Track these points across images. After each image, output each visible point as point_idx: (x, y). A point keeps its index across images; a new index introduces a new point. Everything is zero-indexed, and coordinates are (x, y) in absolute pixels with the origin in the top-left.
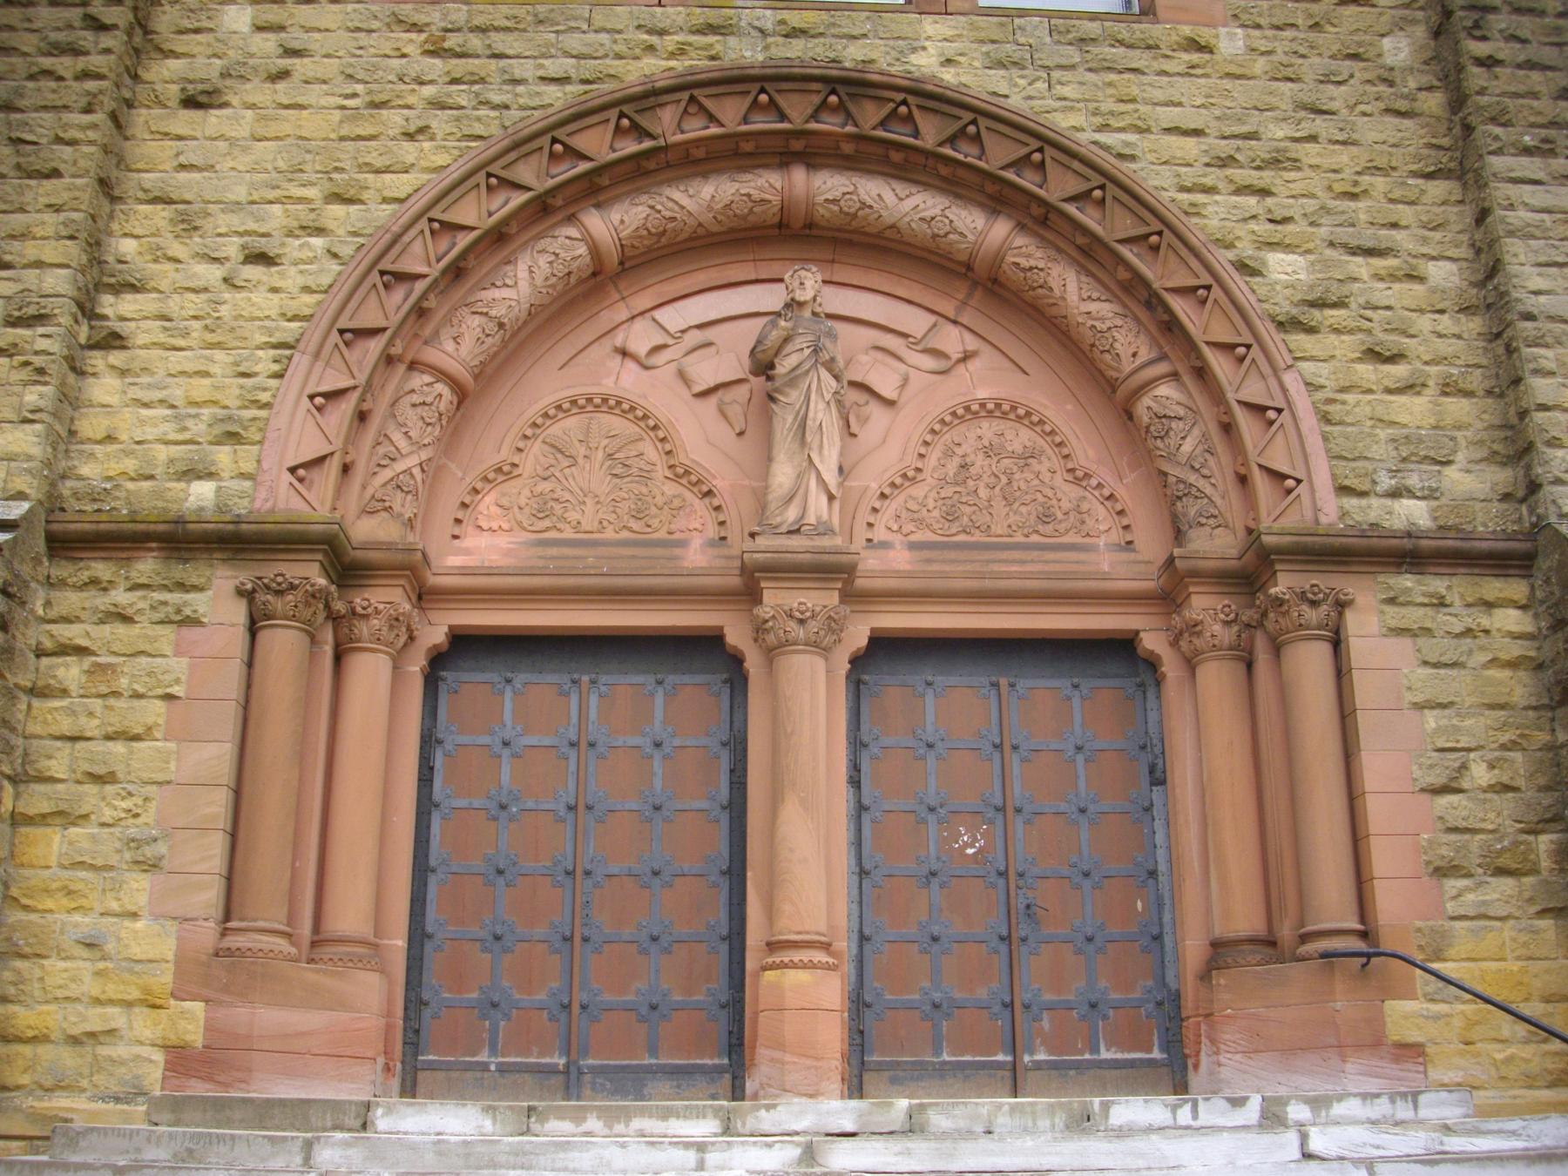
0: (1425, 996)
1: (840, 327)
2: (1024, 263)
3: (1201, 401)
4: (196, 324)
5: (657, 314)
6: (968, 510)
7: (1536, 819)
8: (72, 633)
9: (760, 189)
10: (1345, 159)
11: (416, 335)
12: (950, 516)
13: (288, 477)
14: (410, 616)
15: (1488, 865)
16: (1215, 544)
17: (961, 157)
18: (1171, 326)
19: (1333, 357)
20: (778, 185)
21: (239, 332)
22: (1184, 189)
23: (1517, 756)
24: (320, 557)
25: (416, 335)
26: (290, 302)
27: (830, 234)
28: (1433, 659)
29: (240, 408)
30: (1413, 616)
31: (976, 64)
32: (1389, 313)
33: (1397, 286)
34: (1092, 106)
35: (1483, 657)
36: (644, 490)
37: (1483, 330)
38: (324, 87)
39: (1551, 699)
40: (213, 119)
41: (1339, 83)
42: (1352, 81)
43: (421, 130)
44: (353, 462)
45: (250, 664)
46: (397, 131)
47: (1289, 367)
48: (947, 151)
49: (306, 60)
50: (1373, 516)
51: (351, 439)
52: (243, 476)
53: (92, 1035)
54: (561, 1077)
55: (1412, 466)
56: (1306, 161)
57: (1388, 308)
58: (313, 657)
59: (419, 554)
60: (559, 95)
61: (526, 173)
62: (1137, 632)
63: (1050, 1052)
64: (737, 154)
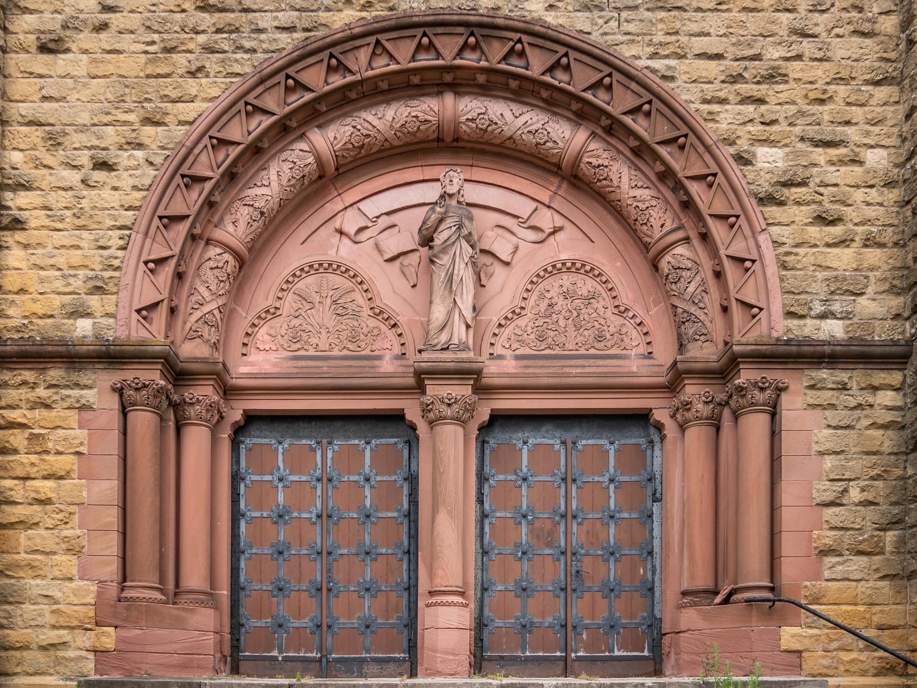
0: (805, 624)
1: (475, 212)
2: (595, 162)
4: (68, 213)
5: (361, 205)
6: (552, 334)
7: (886, 522)
8: (14, 415)
9: (424, 112)
10: (820, 72)
11: (209, 221)
12: (541, 338)
13: (135, 316)
14: (218, 404)
15: (853, 549)
16: (705, 353)
17: (556, 83)
18: (688, 205)
19: (793, 222)
20: (436, 109)
21: (96, 219)
22: (705, 101)
23: (880, 484)
24: (160, 367)
25: (209, 221)
26: (126, 197)
27: (470, 145)
28: (834, 424)
29: (102, 270)
30: (825, 396)
31: (570, 8)
32: (835, 189)
33: (843, 169)
34: (647, 38)
35: (866, 422)
36: (356, 324)
37: (899, 199)
38: (132, 36)
39: (907, 448)
40: (61, 62)
41: (823, 11)
42: (832, 10)
43: (200, 69)
44: (176, 306)
45: (125, 433)
46: (184, 70)
47: (763, 230)
48: (547, 78)
49: (118, 15)
50: (807, 331)
51: (174, 291)
52: (108, 315)
53: (53, 645)
54: (318, 664)
55: (837, 297)
56: (792, 75)
57: (836, 185)
58: (162, 429)
59: (221, 365)
60: (289, 41)
61: (270, 101)
62: (651, 410)
63: (586, 651)
64: (409, 86)
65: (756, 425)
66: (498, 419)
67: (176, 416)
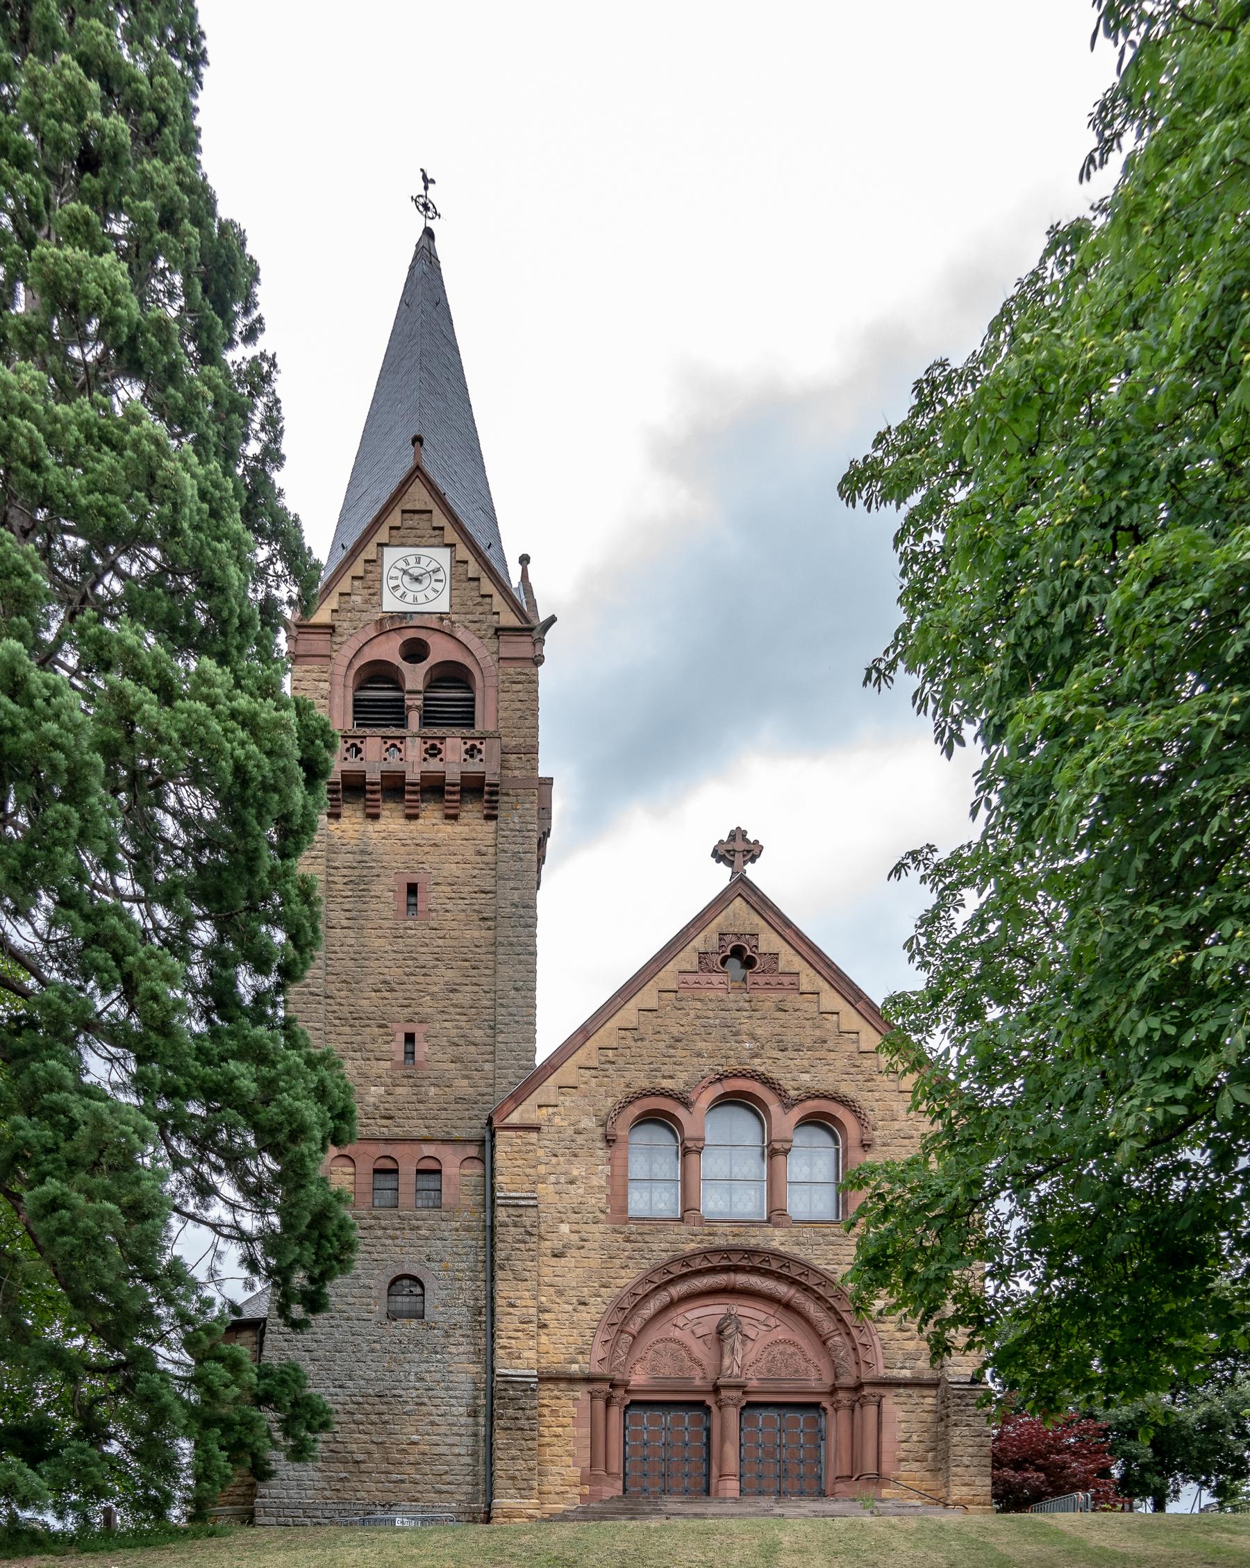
3: (847, 1341)
8: (545, 1402)
12: (769, 1371)
16: (847, 1380)
18: (841, 1320)
30: (902, 1400)
61: (656, 1279)
65: (871, 1410)
66: (751, 1405)
67: (608, 1402)
